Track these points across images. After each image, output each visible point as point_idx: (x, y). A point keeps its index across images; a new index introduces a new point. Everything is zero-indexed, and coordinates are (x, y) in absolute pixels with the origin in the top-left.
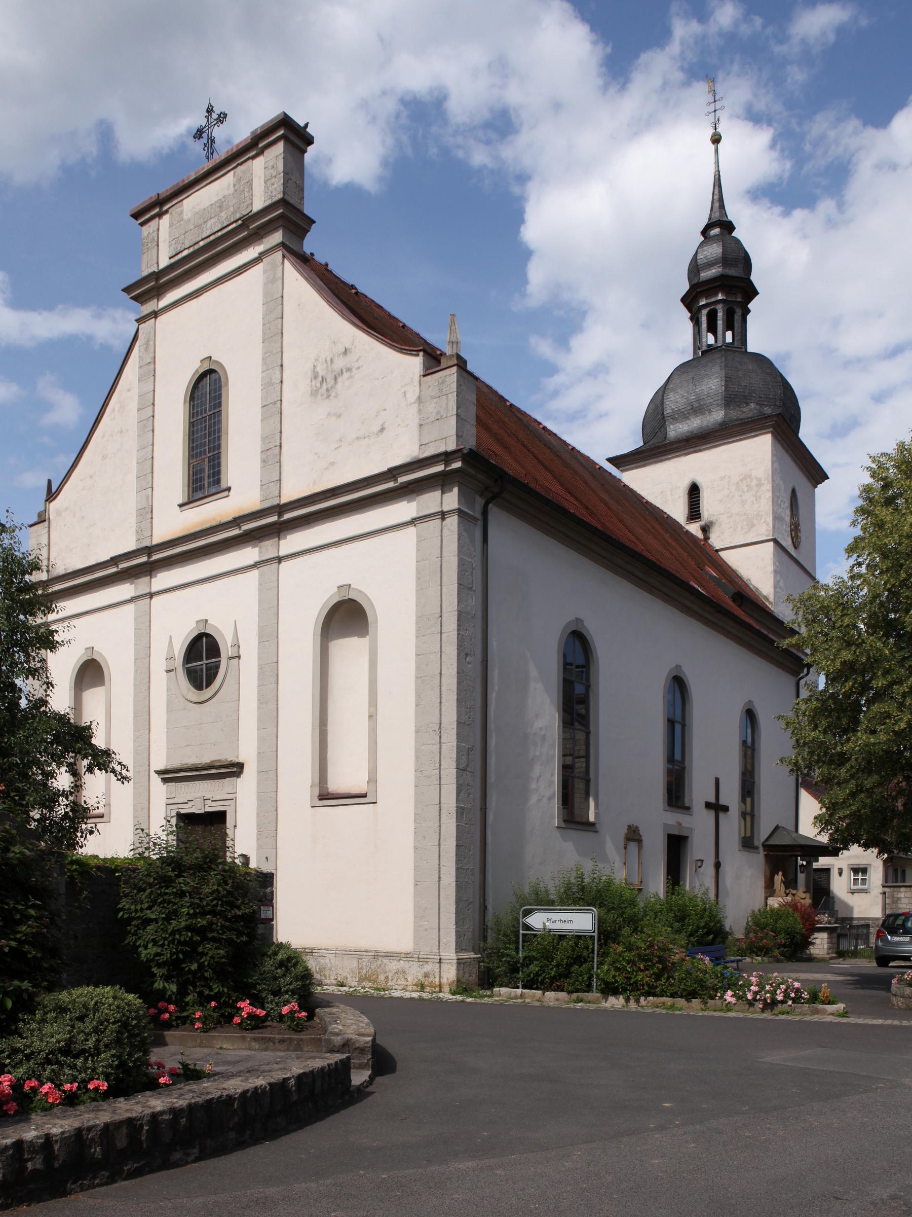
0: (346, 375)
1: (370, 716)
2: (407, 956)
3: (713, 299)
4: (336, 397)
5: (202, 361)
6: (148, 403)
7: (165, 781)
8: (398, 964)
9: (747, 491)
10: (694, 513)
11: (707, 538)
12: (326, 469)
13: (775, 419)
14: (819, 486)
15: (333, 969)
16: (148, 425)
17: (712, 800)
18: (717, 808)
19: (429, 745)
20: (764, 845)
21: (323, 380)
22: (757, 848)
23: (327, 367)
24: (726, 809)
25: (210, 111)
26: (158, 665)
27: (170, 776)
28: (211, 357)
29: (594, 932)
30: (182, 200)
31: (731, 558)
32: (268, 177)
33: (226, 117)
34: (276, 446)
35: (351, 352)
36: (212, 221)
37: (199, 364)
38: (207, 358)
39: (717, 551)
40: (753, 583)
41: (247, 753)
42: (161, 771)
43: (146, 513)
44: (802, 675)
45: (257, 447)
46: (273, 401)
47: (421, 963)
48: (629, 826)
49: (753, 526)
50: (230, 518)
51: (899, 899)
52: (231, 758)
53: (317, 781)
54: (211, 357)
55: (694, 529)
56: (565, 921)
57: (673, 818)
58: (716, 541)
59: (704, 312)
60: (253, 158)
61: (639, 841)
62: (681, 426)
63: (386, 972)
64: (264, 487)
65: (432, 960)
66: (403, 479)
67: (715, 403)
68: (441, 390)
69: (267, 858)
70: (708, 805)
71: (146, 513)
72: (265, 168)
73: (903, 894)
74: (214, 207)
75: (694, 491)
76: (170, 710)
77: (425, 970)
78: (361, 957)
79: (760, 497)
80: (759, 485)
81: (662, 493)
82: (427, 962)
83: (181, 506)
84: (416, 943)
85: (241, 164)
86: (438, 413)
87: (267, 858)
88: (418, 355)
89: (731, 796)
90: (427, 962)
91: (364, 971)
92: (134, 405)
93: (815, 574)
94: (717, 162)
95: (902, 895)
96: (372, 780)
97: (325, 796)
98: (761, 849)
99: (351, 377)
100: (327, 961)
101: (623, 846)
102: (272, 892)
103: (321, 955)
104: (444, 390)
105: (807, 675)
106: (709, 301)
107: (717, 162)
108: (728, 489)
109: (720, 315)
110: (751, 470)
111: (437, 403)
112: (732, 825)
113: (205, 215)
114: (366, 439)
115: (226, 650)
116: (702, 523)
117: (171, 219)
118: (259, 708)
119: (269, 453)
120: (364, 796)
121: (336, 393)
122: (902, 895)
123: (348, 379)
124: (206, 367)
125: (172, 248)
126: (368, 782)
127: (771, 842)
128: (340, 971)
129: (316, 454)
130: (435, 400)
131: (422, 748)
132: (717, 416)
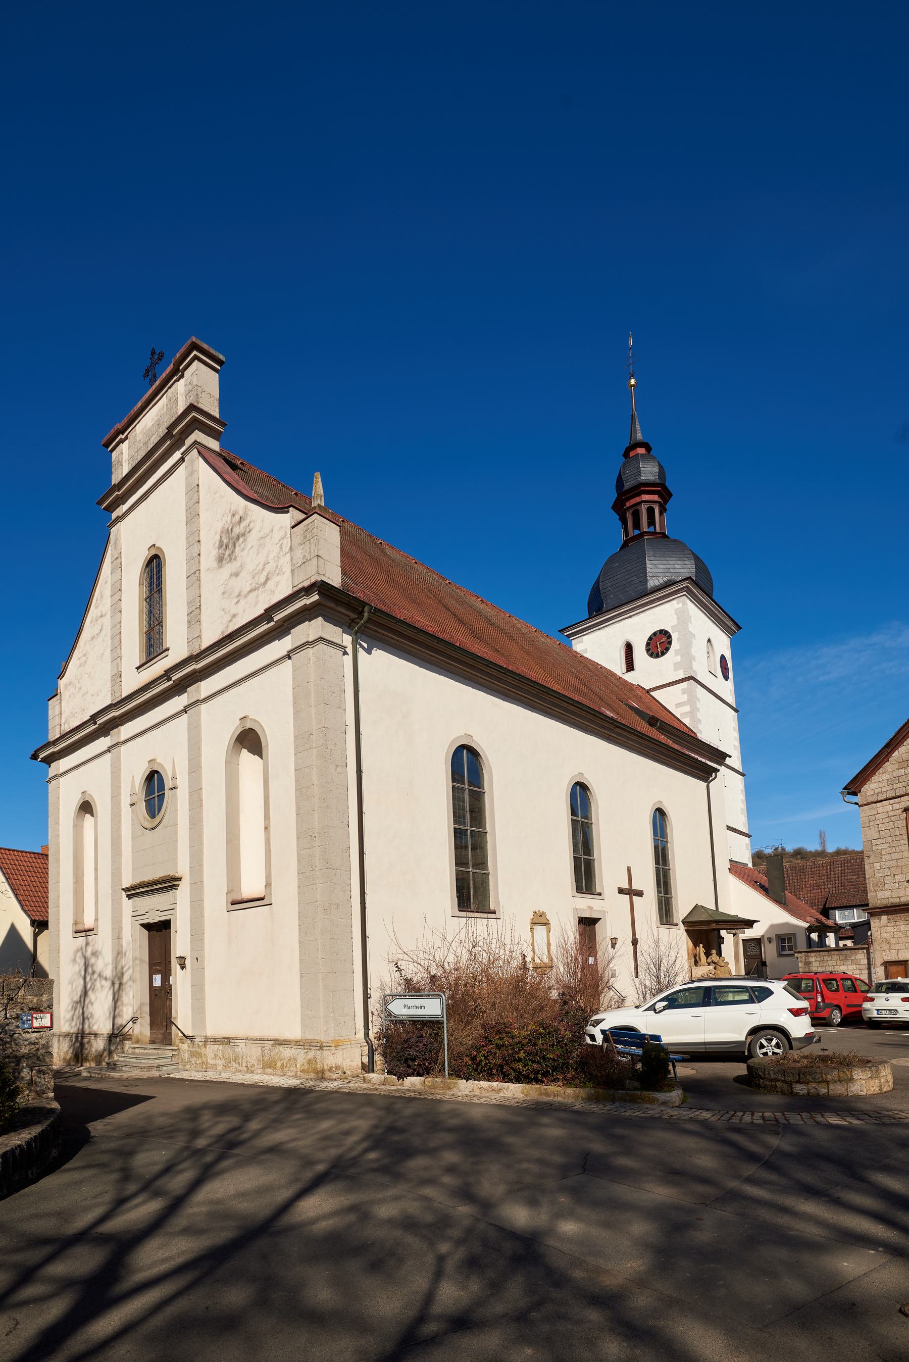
0: (241, 540)
1: (266, 828)
2: (297, 1043)
4: (235, 559)
5: (148, 549)
6: (117, 590)
7: (129, 897)
8: (290, 1051)
12: (230, 621)
15: (244, 1057)
16: (117, 609)
17: (626, 886)
18: (631, 892)
19: (307, 849)
20: (683, 922)
21: (227, 547)
22: (677, 925)
23: (229, 536)
24: (640, 894)
25: (153, 353)
26: (125, 800)
27: (133, 892)
28: (154, 545)
29: (442, 1017)
30: (135, 426)
32: (187, 392)
33: (163, 356)
34: (196, 608)
35: (244, 520)
36: (154, 436)
37: (147, 552)
38: (152, 546)
39: (648, 691)
41: (182, 868)
42: (127, 888)
43: (117, 677)
44: (711, 778)
45: (185, 611)
46: (193, 572)
47: (306, 1051)
48: (535, 912)
50: (163, 673)
51: (810, 963)
52: (172, 873)
54: (154, 545)
56: (418, 1007)
57: (587, 905)
60: (178, 380)
61: (547, 924)
63: (282, 1060)
64: (190, 644)
65: (314, 1048)
66: (277, 617)
68: (305, 537)
69: (197, 959)
70: (640, 894)
71: (117, 677)
72: (185, 385)
74: (155, 426)
76: (134, 838)
77: (309, 1057)
78: (263, 1045)
82: (310, 1049)
83: (138, 668)
84: (303, 1032)
85: (169, 388)
86: (304, 556)
87: (197, 959)
88: (288, 512)
89: (646, 880)
90: (310, 1049)
91: (266, 1058)
92: (108, 593)
95: (813, 959)
96: (268, 885)
97: (237, 903)
98: (681, 925)
99: (244, 540)
100: (240, 1049)
101: (529, 930)
102: (51, 1000)
103: (235, 1044)
104: (308, 537)
105: (715, 777)
111: (303, 548)
112: (648, 905)
113: (149, 433)
114: (256, 591)
115: (168, 784)
117: (129, 443)
118: (190, 829)
119: (192, 615)
120: (262, 899)
121: (235, 556)
122: (813, 959)
123: (243, 543)
124: (153, 552)
125: (130, 465)
126: (265, 886)
127: (691, 920)
128: (249, 1060)
129: (223, 610)
130: (301, 547)
131: (302, 852)
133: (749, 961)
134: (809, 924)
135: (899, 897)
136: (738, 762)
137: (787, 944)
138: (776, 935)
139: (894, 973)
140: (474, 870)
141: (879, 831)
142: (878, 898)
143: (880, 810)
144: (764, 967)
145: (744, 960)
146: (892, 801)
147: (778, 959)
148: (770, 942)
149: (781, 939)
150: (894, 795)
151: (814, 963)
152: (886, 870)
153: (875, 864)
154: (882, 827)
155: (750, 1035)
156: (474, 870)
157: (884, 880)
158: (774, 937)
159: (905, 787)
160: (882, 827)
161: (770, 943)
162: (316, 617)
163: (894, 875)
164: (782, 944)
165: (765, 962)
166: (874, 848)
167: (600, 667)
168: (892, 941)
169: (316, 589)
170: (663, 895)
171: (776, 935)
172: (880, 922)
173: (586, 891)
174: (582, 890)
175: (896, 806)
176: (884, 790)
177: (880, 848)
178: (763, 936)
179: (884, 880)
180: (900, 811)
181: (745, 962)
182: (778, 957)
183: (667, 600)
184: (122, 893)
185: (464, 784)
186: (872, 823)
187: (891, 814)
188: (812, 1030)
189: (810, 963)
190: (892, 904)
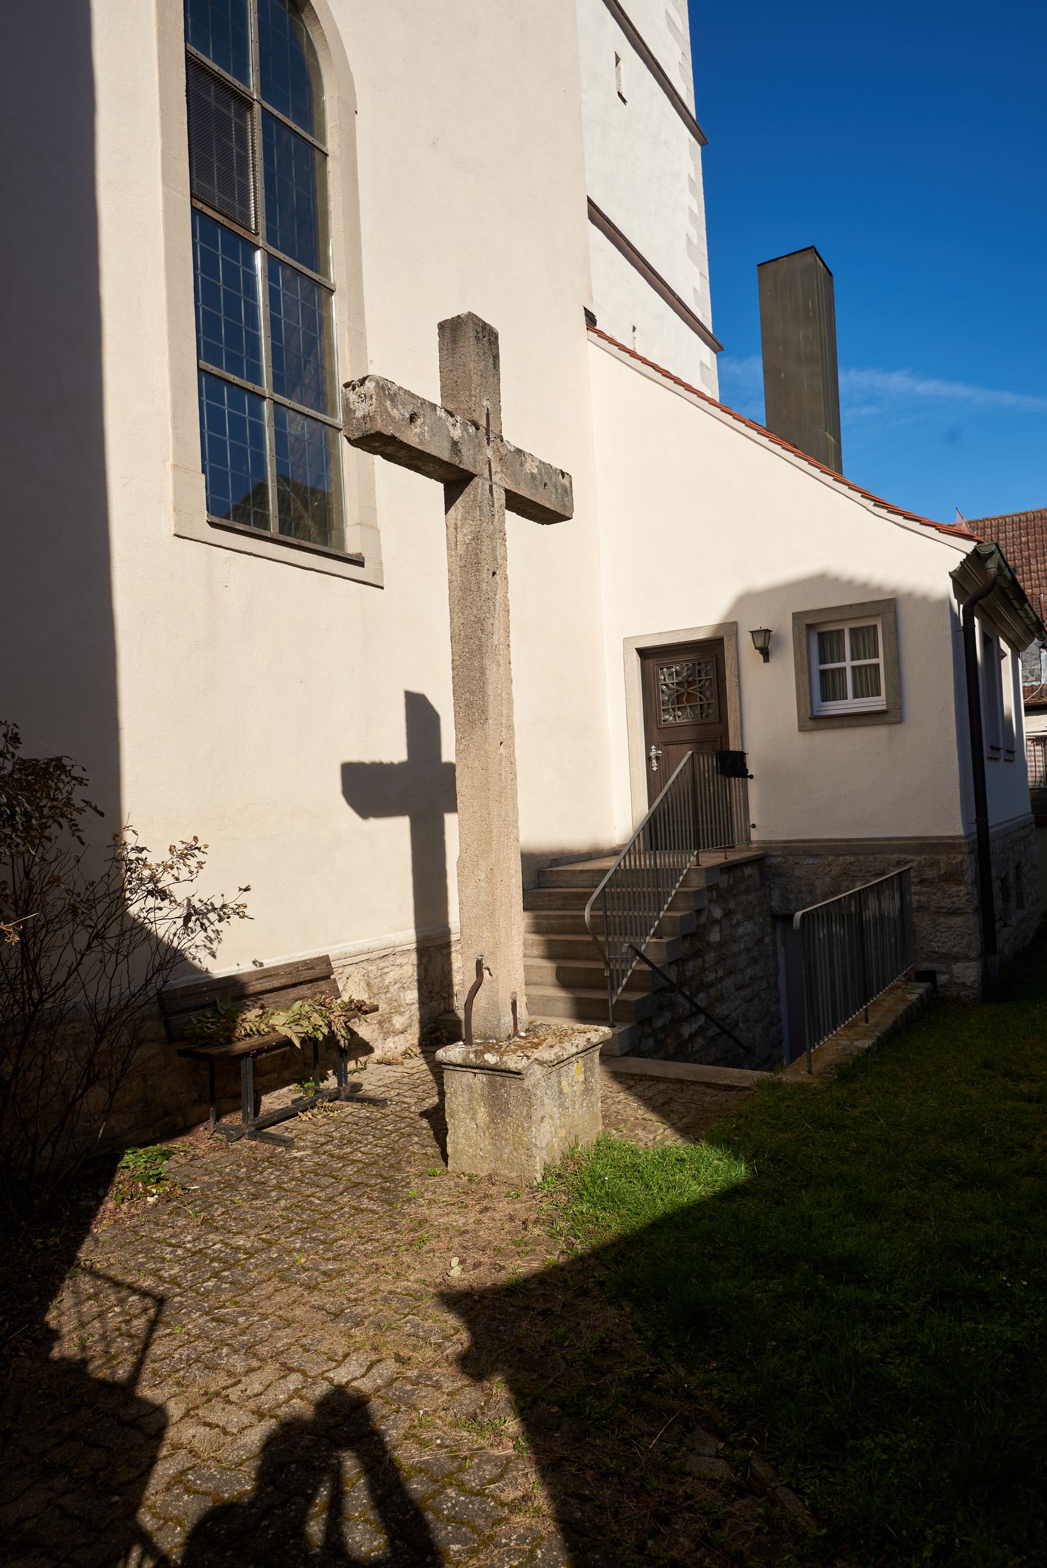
133: (666, 753)
134: (970, 546)
136: (691, 164)
137: (848, 664)
138: (796, 616)
139: (604, 1132)
145: (648, 750)
147: (801, 735)
148: (765, 653)
149: (821, 636)
155: (839, 469)
158: (784, 628)
161: (766, 660)
162: (446, 763)
164: (823, 661)
165: (741, 756)
171: (796, 616)
173: (281, 532)
174: (263, 522)
178: (729, 628)
181: (649, 759)
182: (802, 729)
185: (207, 403)
188: (345, 998)
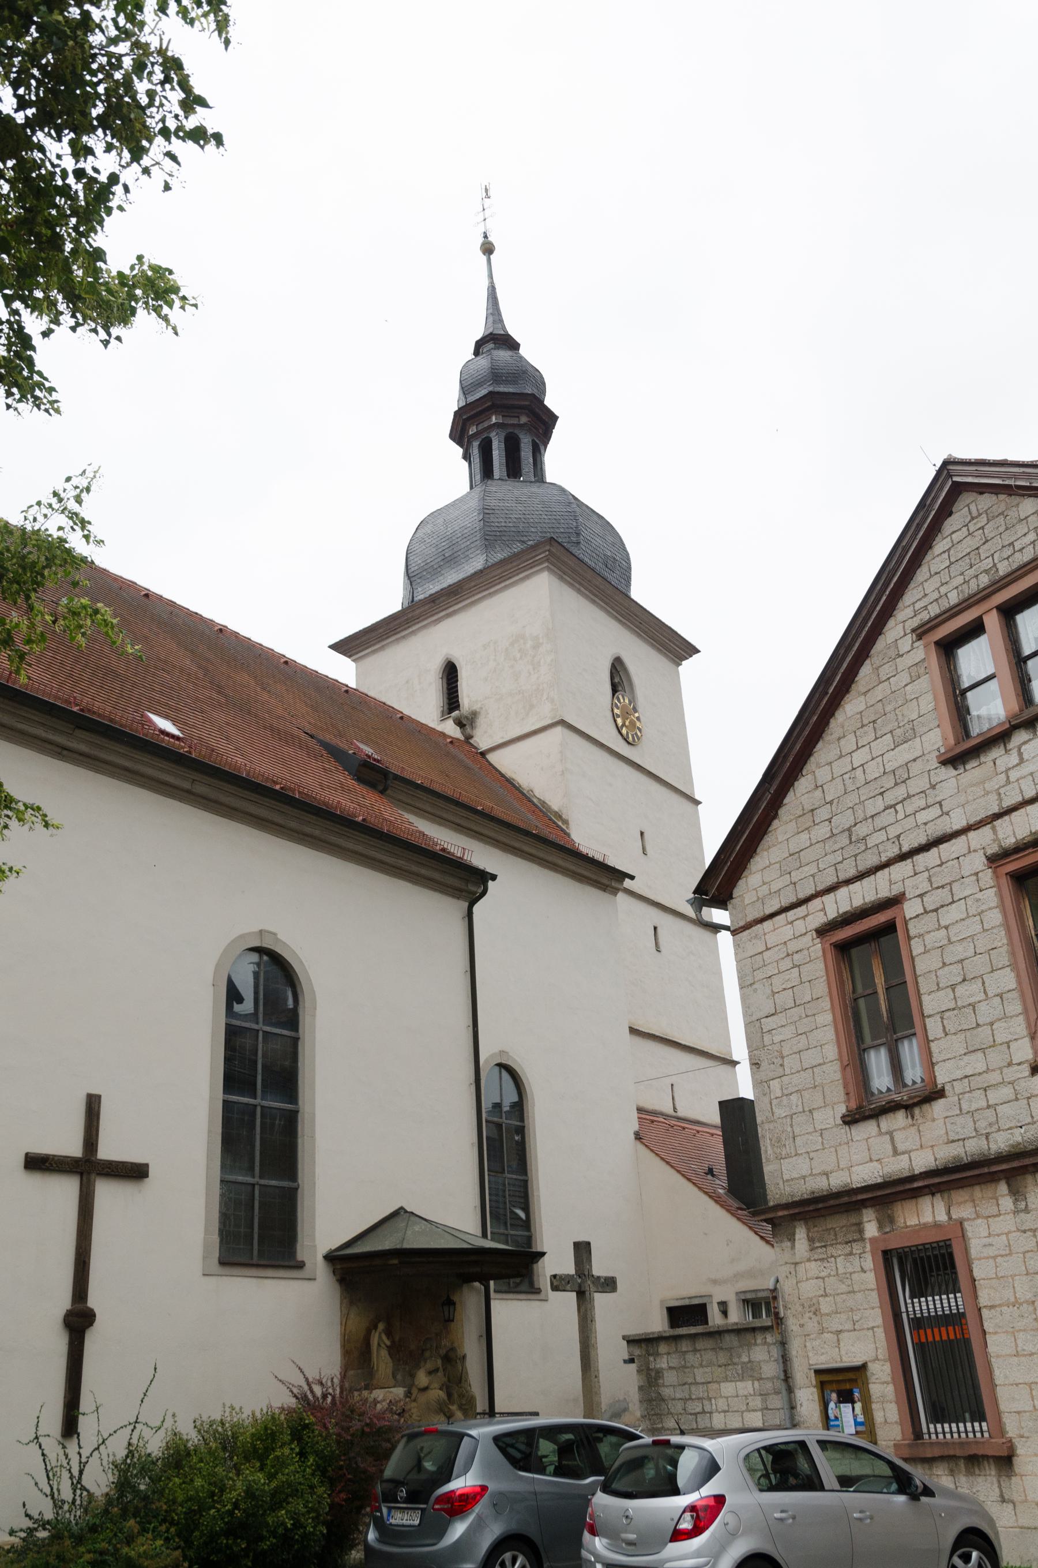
3: (486, 424)
9: (521, 658)
10: (452, 700)
11: (468, 737)
13: (548, 548)
14: (684, 663)
31: (504, 761)
40: (537, 794)
49: (532, 707)
51: (659, 1373)
53: (721, 1329)
55: (450, 728)
58: (483, 740)
59: (476, 444)
62: (431, 587)
67: (472, 545)
73: (665, 1358)
75: (450, 673)
79: (539, 662)
80: (536, 646)
81: (407, 682)
93: (694, 794)
94: (491, 276)
95: (662, 1363)
106: (480, 427)
107: (491, 276)
108: (495, 660)
109: (495, 444)
110: (524, 627)
116: (456, 713)
122: (662, 1363)
132: (477, 563)
135: (826, 1174)
140: (268, 1029)
141: (774, 993)
142: (785, 1177)
143: (772, 939)
144: (446, 1308)
146: (791, 915)
150: (793, 899)
151: (666, 1374)
152: (794, 1098)
153: (771, 1082)
154: (778, 983)
156: (268, 1029)
157: (792, 1126)
159: (813, 876)
160: (778, 983)
163: (810, 1111)
166: (767, 1039)
167: (399, 715)
168: (825, 1306)
169: (84, 240)
170: (256, 1180)
172: (793, 1247)
175: (800, 926)
176: (775, 887)
177: (777, 1039)
179: (792, 1126)
180: (808, 937)
183: (469, 601)
184: (757, 1083)
186: (759, 975)
187: (793, 946)
189: (659, 1373)
190: (813, 1193)
